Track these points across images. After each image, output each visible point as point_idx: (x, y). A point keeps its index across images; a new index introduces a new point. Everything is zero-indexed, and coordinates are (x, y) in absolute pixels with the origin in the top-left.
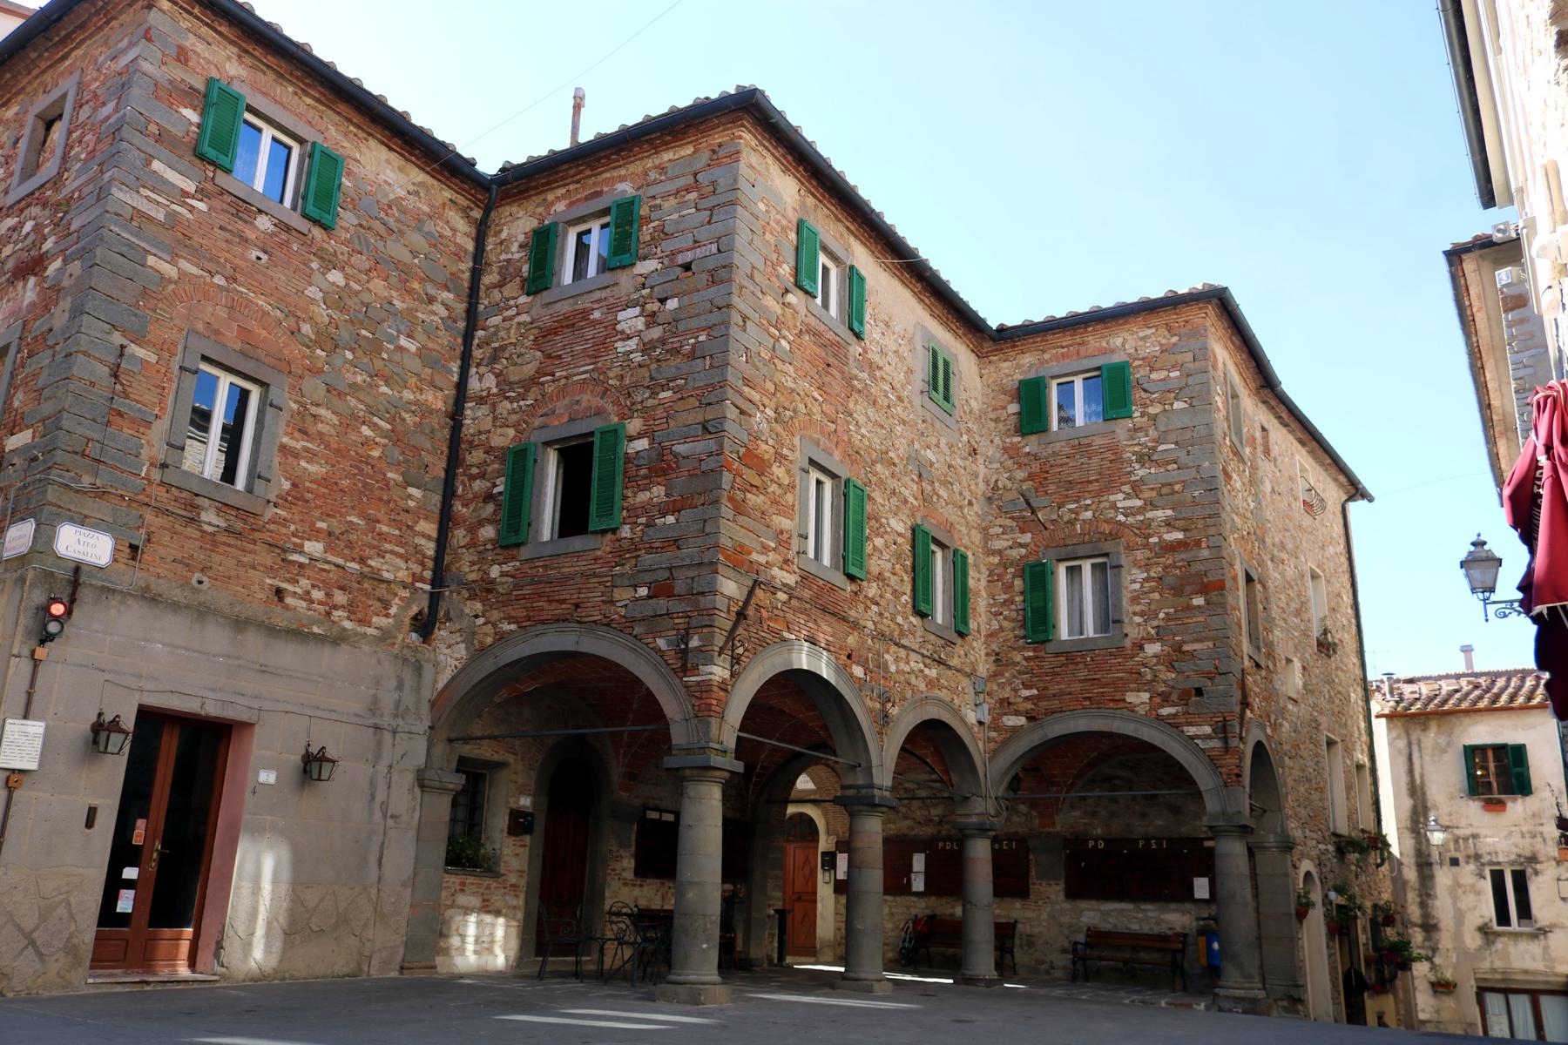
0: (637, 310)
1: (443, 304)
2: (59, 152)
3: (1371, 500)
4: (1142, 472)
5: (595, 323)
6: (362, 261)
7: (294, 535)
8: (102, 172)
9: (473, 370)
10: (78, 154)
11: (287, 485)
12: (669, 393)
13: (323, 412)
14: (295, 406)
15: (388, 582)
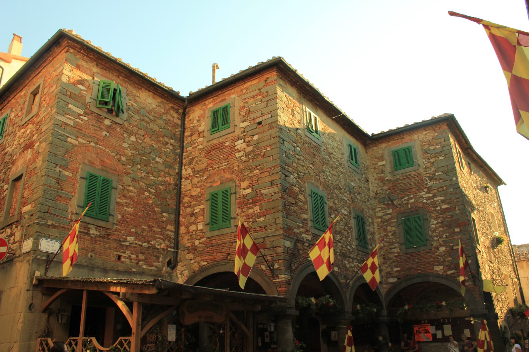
0: (243, 141)
1: (171, 145)
2: (38, 105)
3: (505, 184)
4: (431, 183)
5: (227, 147)
6: (141, 132)
7: (124, 235)
8: (52, 110)
9: (183, 167)
10: (44, 105)
11: (120, 217)
12: (258, 171)
13: (131, 188)
14: (121, 187)
15: (158, 249)
